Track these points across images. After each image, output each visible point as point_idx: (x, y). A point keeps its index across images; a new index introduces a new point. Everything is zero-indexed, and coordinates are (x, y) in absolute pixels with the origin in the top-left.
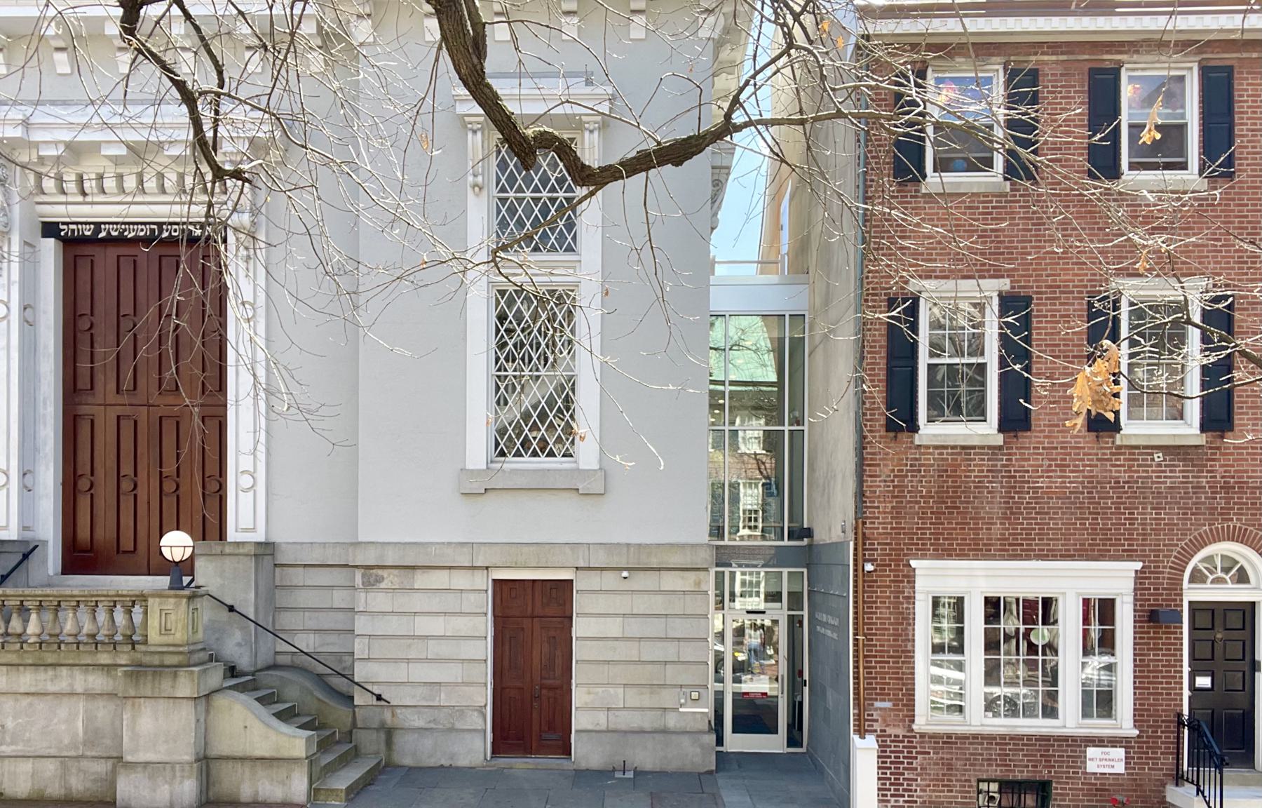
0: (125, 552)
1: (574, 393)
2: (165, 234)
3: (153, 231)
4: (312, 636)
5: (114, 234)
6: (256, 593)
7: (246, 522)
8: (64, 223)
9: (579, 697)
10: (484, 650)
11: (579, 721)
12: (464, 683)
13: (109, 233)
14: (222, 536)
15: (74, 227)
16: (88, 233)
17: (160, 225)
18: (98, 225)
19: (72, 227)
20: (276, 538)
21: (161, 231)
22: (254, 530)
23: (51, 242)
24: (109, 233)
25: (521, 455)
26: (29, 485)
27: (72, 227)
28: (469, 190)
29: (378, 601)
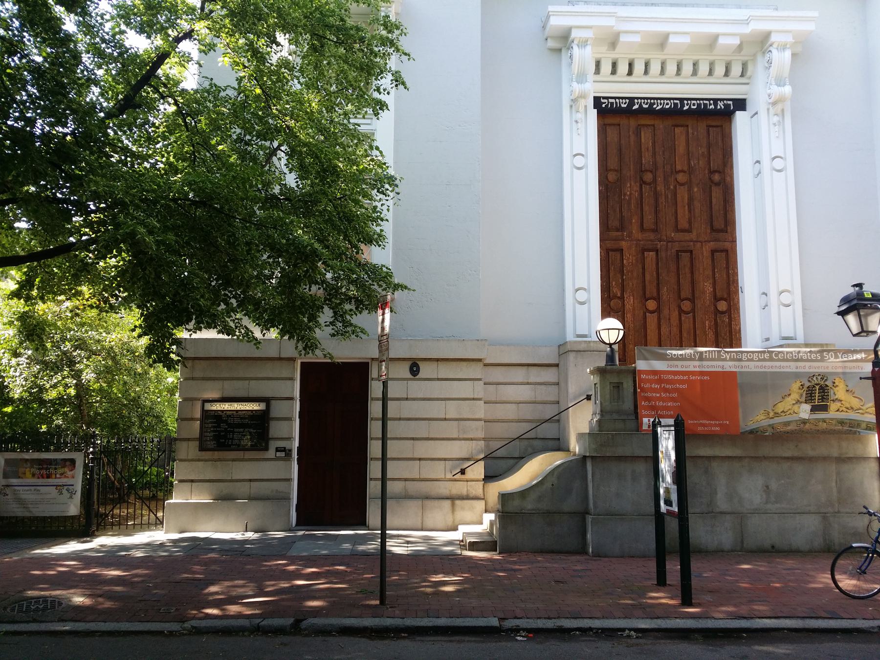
2: (686, 108)
3: (676, 104)
5: (645, 106)
13: (641, 106)
15: (613, 101)
16: (623, 106)
18: (632, 99)
19: (610, 100)
24: (641, 106)
27: (610, 100)
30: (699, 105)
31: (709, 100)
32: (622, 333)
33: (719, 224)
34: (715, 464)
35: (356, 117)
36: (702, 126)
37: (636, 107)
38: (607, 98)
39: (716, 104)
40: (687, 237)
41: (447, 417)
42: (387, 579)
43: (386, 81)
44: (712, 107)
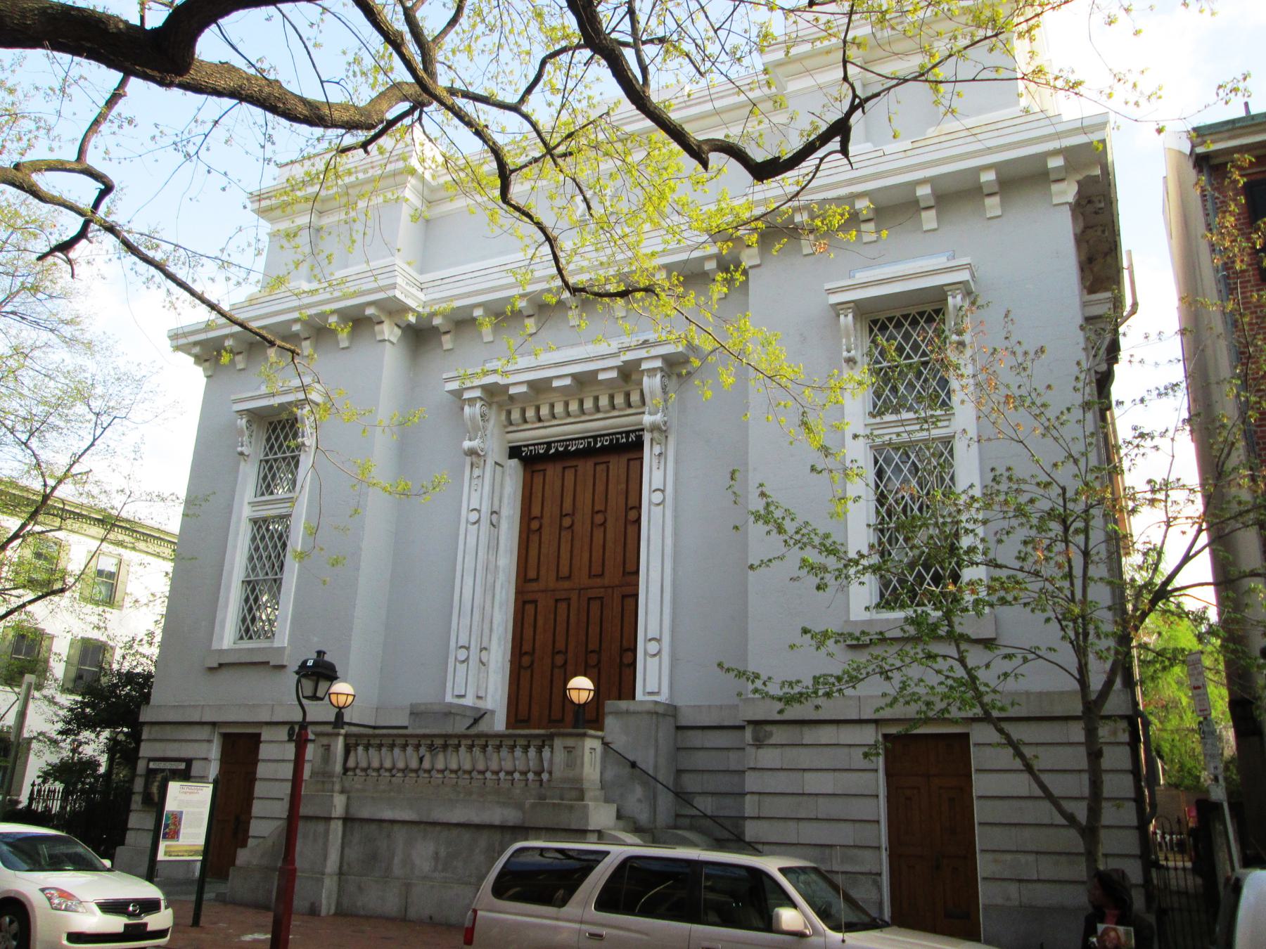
0: (629, 573)
1: (953, 458)
2: (599, 445)
3: (589, 443)
4: (710, 799)
5: (561, 449)
6: (657, 751)
7: (652, 685)
8: (525, 446)
9: (984, 866)
10: (881, 809)
11: (986, 894)
12: (855, 846)
13: (557, 449)
14: (634, 698)
15: (532, 448)
16: (541, 451)
17: (595, 437)
18: (549, 444)
19: (530, 448)
20: (679, 703)
21: (596, 443)
22: (658, 693)
23: (515, 462)
24: (557, 449)
25: (918, 313)
26: (484, 660)
27: (530, 448)
28: (844, 365)
29: (767, 757)
30: (611, 440)
31: (621, 433)
32: (592, 693)
33: (630, 568)
34: (396, 827)
35: (937, 427)
36: (590, 464)
37: (553, 451)
38: (527, 446)
39: (627, 438)
40: (566, 584)
41: (761, 815)
42: (269, 936)
43: (1085, 365)
44: (624, 440)
